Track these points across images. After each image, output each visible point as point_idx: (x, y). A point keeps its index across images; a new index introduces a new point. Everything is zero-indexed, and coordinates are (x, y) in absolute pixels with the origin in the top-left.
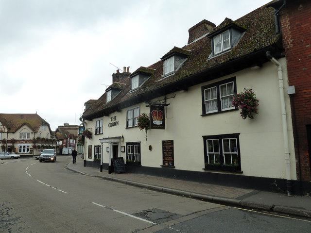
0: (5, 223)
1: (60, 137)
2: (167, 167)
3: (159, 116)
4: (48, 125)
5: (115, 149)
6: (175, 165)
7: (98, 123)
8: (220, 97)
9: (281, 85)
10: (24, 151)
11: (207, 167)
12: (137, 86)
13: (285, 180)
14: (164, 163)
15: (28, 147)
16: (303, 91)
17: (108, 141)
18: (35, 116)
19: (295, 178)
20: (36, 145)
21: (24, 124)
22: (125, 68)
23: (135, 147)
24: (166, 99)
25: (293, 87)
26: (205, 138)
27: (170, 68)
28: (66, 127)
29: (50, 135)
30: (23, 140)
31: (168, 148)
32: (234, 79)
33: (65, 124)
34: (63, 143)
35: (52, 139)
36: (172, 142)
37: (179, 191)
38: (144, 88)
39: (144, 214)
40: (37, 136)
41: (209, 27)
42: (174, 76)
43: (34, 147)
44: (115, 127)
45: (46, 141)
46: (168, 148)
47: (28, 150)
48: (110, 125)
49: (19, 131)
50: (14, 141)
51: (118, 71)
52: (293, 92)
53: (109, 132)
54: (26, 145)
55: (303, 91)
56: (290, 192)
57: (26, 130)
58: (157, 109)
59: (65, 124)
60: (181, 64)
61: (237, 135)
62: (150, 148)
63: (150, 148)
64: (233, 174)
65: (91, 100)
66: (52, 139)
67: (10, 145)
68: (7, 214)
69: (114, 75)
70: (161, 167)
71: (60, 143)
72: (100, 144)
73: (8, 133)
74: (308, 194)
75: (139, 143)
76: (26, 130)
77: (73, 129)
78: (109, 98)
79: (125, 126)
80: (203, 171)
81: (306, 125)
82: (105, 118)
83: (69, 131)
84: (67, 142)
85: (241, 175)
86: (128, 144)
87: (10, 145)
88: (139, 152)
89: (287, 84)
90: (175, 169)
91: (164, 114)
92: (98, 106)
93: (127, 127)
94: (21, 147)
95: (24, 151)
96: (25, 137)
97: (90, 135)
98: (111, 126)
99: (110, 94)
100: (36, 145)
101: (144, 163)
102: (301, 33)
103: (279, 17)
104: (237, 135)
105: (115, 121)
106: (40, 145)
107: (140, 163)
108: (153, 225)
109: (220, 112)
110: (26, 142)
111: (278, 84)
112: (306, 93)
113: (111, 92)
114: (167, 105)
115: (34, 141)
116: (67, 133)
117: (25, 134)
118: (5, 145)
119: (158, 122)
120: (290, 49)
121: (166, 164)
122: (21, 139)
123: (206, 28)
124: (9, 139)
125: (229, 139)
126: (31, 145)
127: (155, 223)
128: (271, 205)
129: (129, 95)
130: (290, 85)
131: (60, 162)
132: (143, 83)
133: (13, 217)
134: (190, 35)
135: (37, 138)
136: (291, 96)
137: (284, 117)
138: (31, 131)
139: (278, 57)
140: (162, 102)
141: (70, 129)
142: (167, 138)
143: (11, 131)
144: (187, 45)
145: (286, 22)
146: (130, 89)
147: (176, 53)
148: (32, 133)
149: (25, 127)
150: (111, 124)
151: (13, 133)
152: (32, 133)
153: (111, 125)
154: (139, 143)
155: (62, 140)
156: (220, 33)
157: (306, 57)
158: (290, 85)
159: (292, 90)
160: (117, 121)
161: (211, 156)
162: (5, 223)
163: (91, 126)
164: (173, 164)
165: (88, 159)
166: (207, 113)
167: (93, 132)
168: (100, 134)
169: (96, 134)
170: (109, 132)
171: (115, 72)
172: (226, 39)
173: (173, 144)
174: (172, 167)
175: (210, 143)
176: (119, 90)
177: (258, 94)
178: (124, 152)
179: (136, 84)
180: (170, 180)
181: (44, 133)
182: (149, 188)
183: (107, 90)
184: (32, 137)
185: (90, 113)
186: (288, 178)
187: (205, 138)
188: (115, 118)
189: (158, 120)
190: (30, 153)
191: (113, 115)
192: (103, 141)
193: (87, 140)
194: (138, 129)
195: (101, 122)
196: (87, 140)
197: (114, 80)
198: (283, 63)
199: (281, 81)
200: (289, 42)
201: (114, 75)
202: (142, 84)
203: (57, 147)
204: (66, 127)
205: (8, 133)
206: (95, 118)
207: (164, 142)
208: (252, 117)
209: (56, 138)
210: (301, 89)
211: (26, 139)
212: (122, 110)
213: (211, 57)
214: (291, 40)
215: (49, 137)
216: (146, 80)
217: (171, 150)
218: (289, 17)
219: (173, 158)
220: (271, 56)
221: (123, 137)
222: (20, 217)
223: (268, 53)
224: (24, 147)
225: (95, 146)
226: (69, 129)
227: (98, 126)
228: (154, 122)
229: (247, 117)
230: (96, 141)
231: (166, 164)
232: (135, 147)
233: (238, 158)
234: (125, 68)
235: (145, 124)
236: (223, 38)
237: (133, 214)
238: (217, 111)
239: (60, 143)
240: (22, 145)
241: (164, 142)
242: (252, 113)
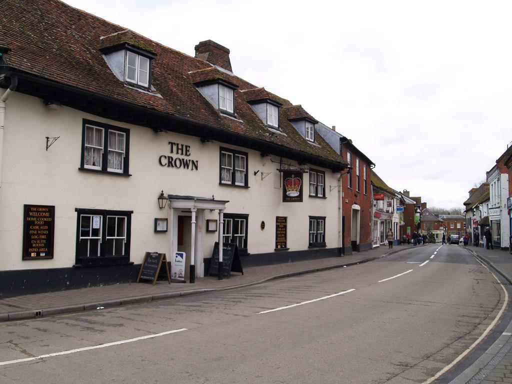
2: (279, 250)
6: (288, 246)
14: (277, 246)
26: (311, 217)
58: (293, 176)
62: (263, 225)
63: (263, 225)
90: (290, 250)
106: (384, 255)
109: (104, 171)
121: (279, 247)
131: (398, 374)
142: (281, 215)
164: (285, 246)
173: (286, 222)
174: (285, 250)
180: (84, 290)
188: (186, 150)
219: (286, 239)
228: (287, 193)
231: (279, 247)
241: (277, 218)
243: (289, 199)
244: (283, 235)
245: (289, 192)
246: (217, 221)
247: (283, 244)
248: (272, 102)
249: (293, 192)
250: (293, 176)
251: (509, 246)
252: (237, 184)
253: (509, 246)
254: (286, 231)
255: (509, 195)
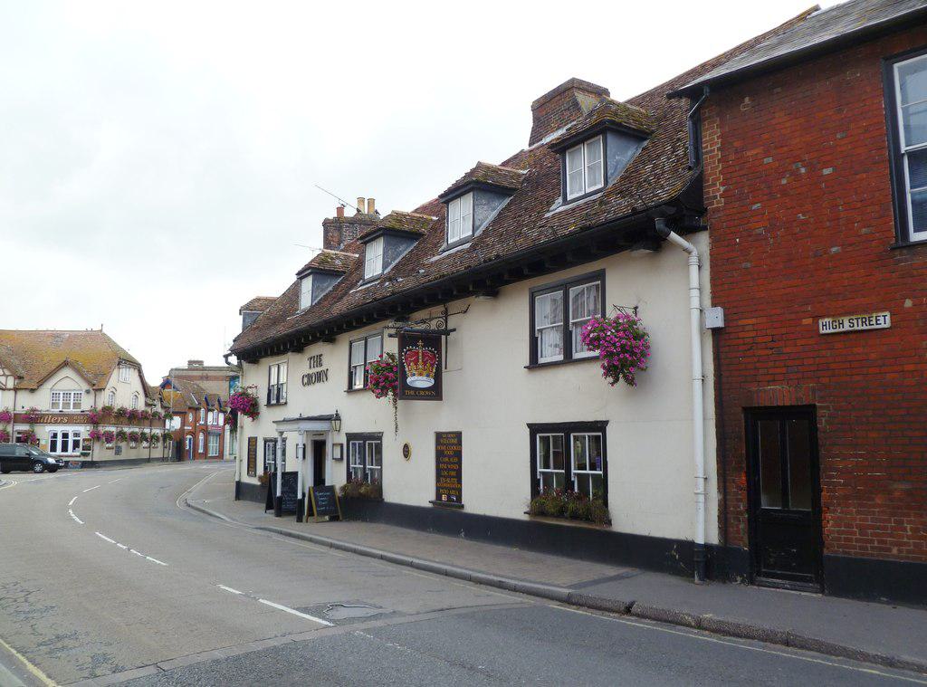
0: (24, 616)
1: (175, 406)
2: (444, 505)
3: (425, 363)
4: (136, 366)
5: (319, 448)
6: (464, 501)
7: (274, 370)
8: (571, 321)
9: (695, 303)
10: (65, 448)
11: (537, 509)
12: (378, 271)
13: (692, 544)
14: (439, 496)
15: (76, 435)
16: (740, 323)
17: (295, 426)
18: (99, 337)
19: (715, 539)
20: (103, 429)
21: (65, 364)
22: (361, 200)
23: (367, 445)
24: (446, 314)
25: (719, 311)
27: (462, 223)
28: (195, 373)
29: (142, 399)
30: (61, 414)
31: (449, 452)
32: (601, 275)
33: (191, 363)
34: (183, 424)
35: (149, 410)
36: (458, 435)
37: (471, 572)
38: (390, 279)
39: (317, 611)
40: (104, 400)
41: (586, 102)
42: (468, 251)
43: (95, 437)
44: (318, 385)
45: (132, 417)
46: (449, 452)
47: (76, 444)
48: (306, 380)
49: (48, 385)
50: (33, 418)
51: (340, 210)
52: (720, 323)
53: (305, 400)
54: (70, 429)
55: (740, 323)
56: (699, 576)
57: (68, 382)
58: (420, 343)
59: (191, 363)
60: (494, 214)
61: (601, 426)
62: (406, 451)
63: (406, 451)
64: (590, 527)
65: (258, 299)
66: (149, 410)
67: (24, 427)
68: (26, 601)
69: (326, 224)
70: (430, 505)
71: (176, 423)
72: (275, 435)
73: (16, 390)
74: (739, 579)
75: (378, 437)
76: (68, 382)
77: (216, 378)
78: (306, 301)
79: (346, 387)
80: (526, 518)
81: (743, 408)
82: (291, 357)
83: (205, 385)
84: (196, 420)
85: (608, 529)
86: (350, 437)
87: (24, 427)
88: (380, 462)
89: (708, 301)
91: (440, 357)
92: (275, 321)
93: (350, 389)
94: (55, 435)
95: (65, 448)
96: (66, 405)
97: (251, 409)
98: (309, 383)
99: (307, 284)
100: (103, 429)
101: (392, 494)
102: (741, 173)
103: (697, 120)
104: (601, 426)
105: (319, 369)
107: (379, 489)
108: (327, 627)
110: (71, 419)
111: (689, 298)
112: (747, 328)
113: (310, 279)
114: (447, 332)
115: (94, 418)
116: (199, 392)
117: (67, 395)
118: (9, 429)
119: (421, 381)
120: (717, 210)
121: (444, 498)
122: (56, 411)
123: (576, 105)
124: (19, 410)
125: (586, 434)
126: (84, 431)
127: (332, 625)
128: (628, 600)
129: (356, 295)
130: (714, 305)
132: (397, 261)
133: (39, 606)
134: (536, 119)
135: (105, 409)
136: (716, 332)
137: (698, 385)
138: (85, 386)
139: (688, 231)
140: (433, 325)
141: (207, 378)
142: (445, 427)
143: (25, 384)
144: (526, 148)
145: (712, 139)
146: (362, 277)
147: (478, 184)
148: (88, 392)
149: (67, 372)
150: (309, 376)
151: (33, 391)
152: (88, 392)
153: (310, 380)
154: (378, 437)
155: (182, 414)
156: (582, 141)
157: (750, 236)
158: (714, 305)
159: (716, 318)
160: (323, 368)
161: (547, 476)
162: (24, 616)
163: (256, 380)
165: (246, 479)
166: (541, 361)
167: (263, 400)
168: (278, 404)
169: (269, 404)
170: (305, 400)
171: (332, 214)
172: (595, 160)
173: (460, 443)
174: (456, 507)
175: (545, 441)
176: (334, 274)
177: (649, 321)
178: (342, 458)
179: (375, 261)
181: (124, 392)
182: (382, 557)
183: (302, 275)
184: (87, 404)
185: (255, 339)
186: (700, 540)
187: (535, 429)
188: (317, 360)
189: (421, 374)
190: (84, 455)
191: (315, 350)
192: (282, 427)
193: (244, 420)
194: (369, 398)
195: (283, 369)
196: (244, 420)
197: (328, 243)
198: (700, 247)
199: (695, 293)
200: (716, 192)
201: (326, 224)
202: (394, 264)
203: (166, 437)
204: (195, 373)
205: (16, 390)
206: (266, 355)
207: (439, 436)
208: (630, 381)
209: (162, 407)
210: (735, 317)
211: (71, 410)
212: (338, 337)
213: (558, 207)
214: (722, 189)
215: (141, 405)
216: (405, 250)
217: (456, 460)
218: (720, 126)
220: (666, 230)
221: (338, 417)
222: (54, 607)
223: (659, 224)
224: (65, 435)
225: (266, 441)
226: (202, 378)
227: (274, 381)
228: (409, 380)
229: (621, 380)
230: (262, 427)
231: (444, 498)
232: (367, 445)
233: (602, 483)
234: (361, 200)
235: (387, 381)
236: (589, 158)
237: (297, 609)
238: (561, 358)
239: (176, 423)
240: (59, 429)
241: (439, 436)
242: (634, 370)
243: (412, 393)
244: (453, 473)
245: (413, 378)
246: (342, 445)
247: (453, 492)
248: (451, 196)
249: (420, 378)
250: (420, 343)
251: (327, 485)
252: (576, 356)
253: (327, 485)
254: (460, 463)
255: (443, 219)
